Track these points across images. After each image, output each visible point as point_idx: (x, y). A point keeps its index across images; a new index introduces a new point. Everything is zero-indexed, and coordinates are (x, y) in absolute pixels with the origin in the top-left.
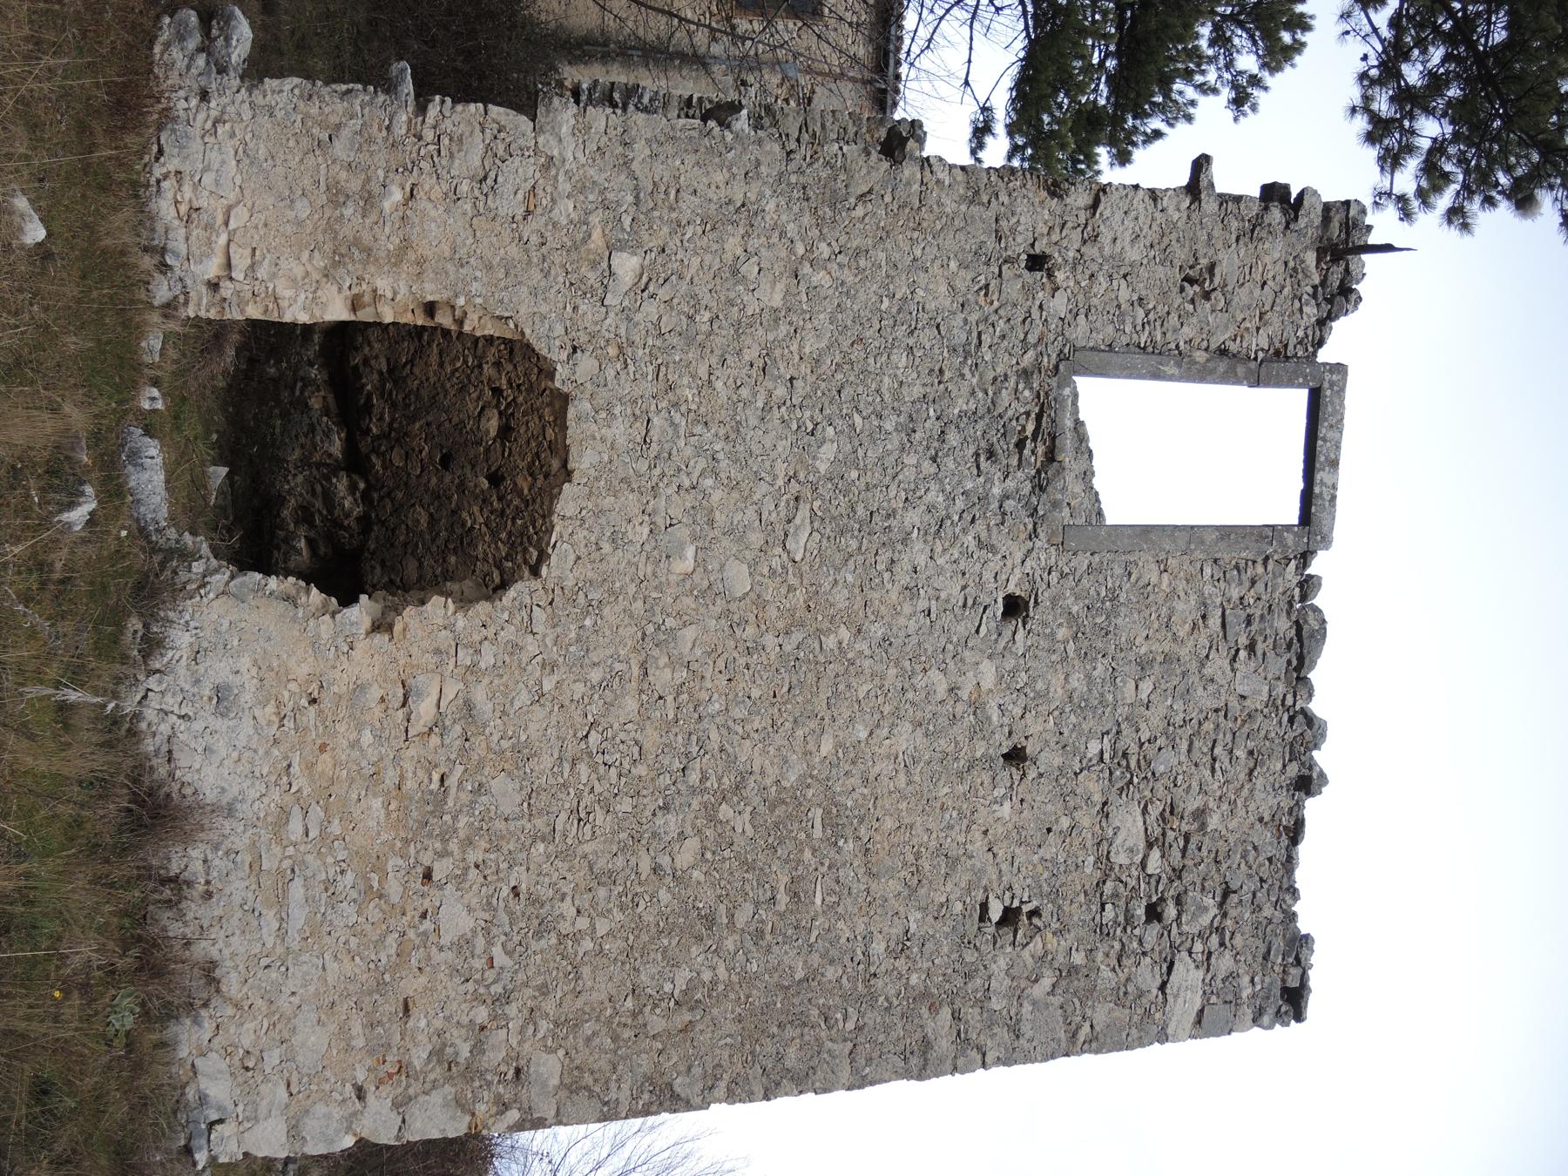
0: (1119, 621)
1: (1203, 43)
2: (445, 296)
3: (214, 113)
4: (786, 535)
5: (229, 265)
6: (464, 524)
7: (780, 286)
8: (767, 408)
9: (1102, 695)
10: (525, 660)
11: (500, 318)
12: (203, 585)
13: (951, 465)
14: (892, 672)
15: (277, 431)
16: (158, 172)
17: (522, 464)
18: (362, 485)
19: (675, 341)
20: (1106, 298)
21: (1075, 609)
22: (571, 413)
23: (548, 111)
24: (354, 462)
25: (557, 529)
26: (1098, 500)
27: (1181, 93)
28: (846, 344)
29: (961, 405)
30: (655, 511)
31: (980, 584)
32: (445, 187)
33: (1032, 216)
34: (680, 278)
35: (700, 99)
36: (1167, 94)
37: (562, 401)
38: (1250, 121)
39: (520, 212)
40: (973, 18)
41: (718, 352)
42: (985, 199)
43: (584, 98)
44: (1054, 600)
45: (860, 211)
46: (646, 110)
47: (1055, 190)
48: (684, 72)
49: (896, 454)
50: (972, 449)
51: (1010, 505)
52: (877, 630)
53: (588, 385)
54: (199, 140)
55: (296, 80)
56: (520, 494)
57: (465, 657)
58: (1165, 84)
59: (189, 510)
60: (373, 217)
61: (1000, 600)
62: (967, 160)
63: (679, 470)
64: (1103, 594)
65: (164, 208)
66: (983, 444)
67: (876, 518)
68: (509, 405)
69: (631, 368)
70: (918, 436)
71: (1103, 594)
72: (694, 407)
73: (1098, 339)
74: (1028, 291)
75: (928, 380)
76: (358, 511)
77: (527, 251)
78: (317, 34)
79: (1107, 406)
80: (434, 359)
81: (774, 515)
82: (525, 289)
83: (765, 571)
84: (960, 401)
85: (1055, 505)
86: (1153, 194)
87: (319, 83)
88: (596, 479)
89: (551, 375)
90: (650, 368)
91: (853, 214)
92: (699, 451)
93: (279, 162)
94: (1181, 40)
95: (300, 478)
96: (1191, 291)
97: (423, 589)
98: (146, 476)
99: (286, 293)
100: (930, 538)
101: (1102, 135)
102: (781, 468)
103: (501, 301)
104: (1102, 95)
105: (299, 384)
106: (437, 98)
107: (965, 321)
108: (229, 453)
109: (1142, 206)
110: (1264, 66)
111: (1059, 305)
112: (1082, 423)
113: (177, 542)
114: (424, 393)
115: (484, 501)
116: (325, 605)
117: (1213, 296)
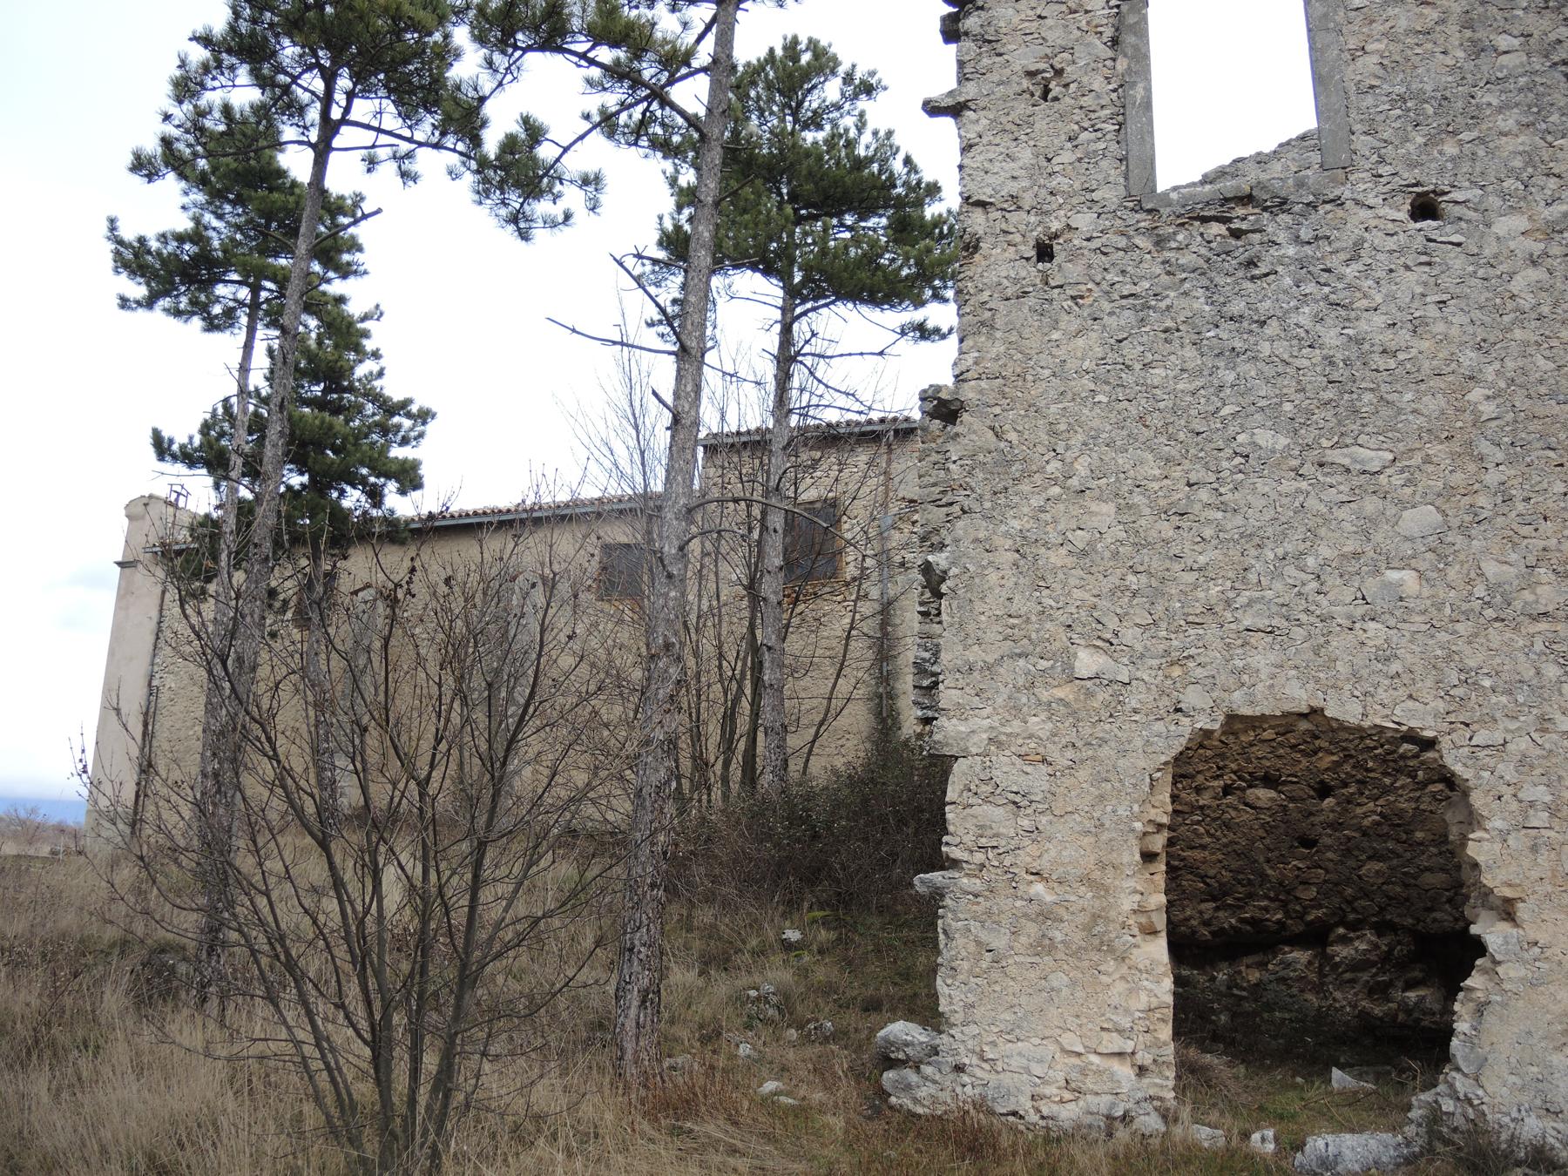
0: (1428, 88)
1: (821, 136)
2: (1135, 842)
3: (975, 1061)
4: (1364, 472)
5: (1120, 1054)
6: (1378, 824)
7: (1094, 507)
8: (1223, 507)
9: (1521, 90)
10: (1539, 752)
11: (1152, 786)
12: (1469, 1101)
13: (1268, 304)
14: (1518, 334)
15: (1287, 1016)
16: (1033, 1118)
17: (1305, 763)
18: (1341, 931)
19: (1159, 609)
20: (1073, 175)
21: (1420, 140)
22: (1246, 711)
23: (947, 744)
24: (1316, 937)
25: (1378, 721)
26: (1288, 143)
27: (867, 147)
28: (1147, 433)
29: (1200, 304)
30: (1349, 617)
31: (1401, 251)
32: (1027, 842)
33: (1000, 264)
34: (1095, 607)
35: (921, 604)
36: (870, 160)
37: (1234, 722)
38: (884, 76)
39: (1044, 768)
40: (823, 357)
41: (1168, 564)
42: (988, 314)
43: (930, 714)
44: (1412, 165)
45: (1012, 436)
46: (936, 654)
47: (972, 247)
48: (898, 621)
49: (1260, 365)
50: (1248, 285)
51: (1305, 234)
52: (1469, 358)
53: (1215, 695)
54: (1001, 1076)
55: (939, 981)
56: (1337, 764)
57: (1540, 818)
58: (860, 164)
59: (1383, 1110)
60: (1062, 912)
61: (1418, 225)
62: (954, 339)
63: (1300, 594)
64: (1398, 112)
65: (1068, 1113)
66: (1240, 274)
67: (1335, 376)
68: (1241, 778)
69: (1193, 651)
70: (1238, 344)
71: (1398, 112)
72: (1229, 584)
73: (1115, 175)
74: (1073, 257)
75: (1176, 343)
76: (1370, 935)
77: (1082, 761)
78: (895, 962)
79: (1183, 157)
80: (1198, 854)
81: (1342, 488)
82: (1121, 762)
83: (1408, 491)
84: (1196, 306)
85: (1300, 184)
86: (966, 149)
87: (940, 960)
88: (1317, 681)
89: (1207, 734)
90: (1191, 632)
91: (1015, 442)
92: (1276, 574)
93: (1016, 1001)
94: (820, 158)
95: (1338, 995)
96: (1056, 89)
97: (1458, 867)
98: (1347, 1153)
99: (1143, 1000)
100: (1353, 314)
101: (914, 215)
102: (1288, 486)
103: (1135, 785)
104: (878, 222)
105: (1235, 991)
106: (944, 849)
107: (1111, 314)
108: (1318, 1066)
109: (980, 158)
110: (833, 73)
111: (1085, 221)
112: (1205, 176)
113: (1420, 1125)
114: (1235, 865)
115: (1349, 802)
116: (1485, 971)
117: (1058, 66)
